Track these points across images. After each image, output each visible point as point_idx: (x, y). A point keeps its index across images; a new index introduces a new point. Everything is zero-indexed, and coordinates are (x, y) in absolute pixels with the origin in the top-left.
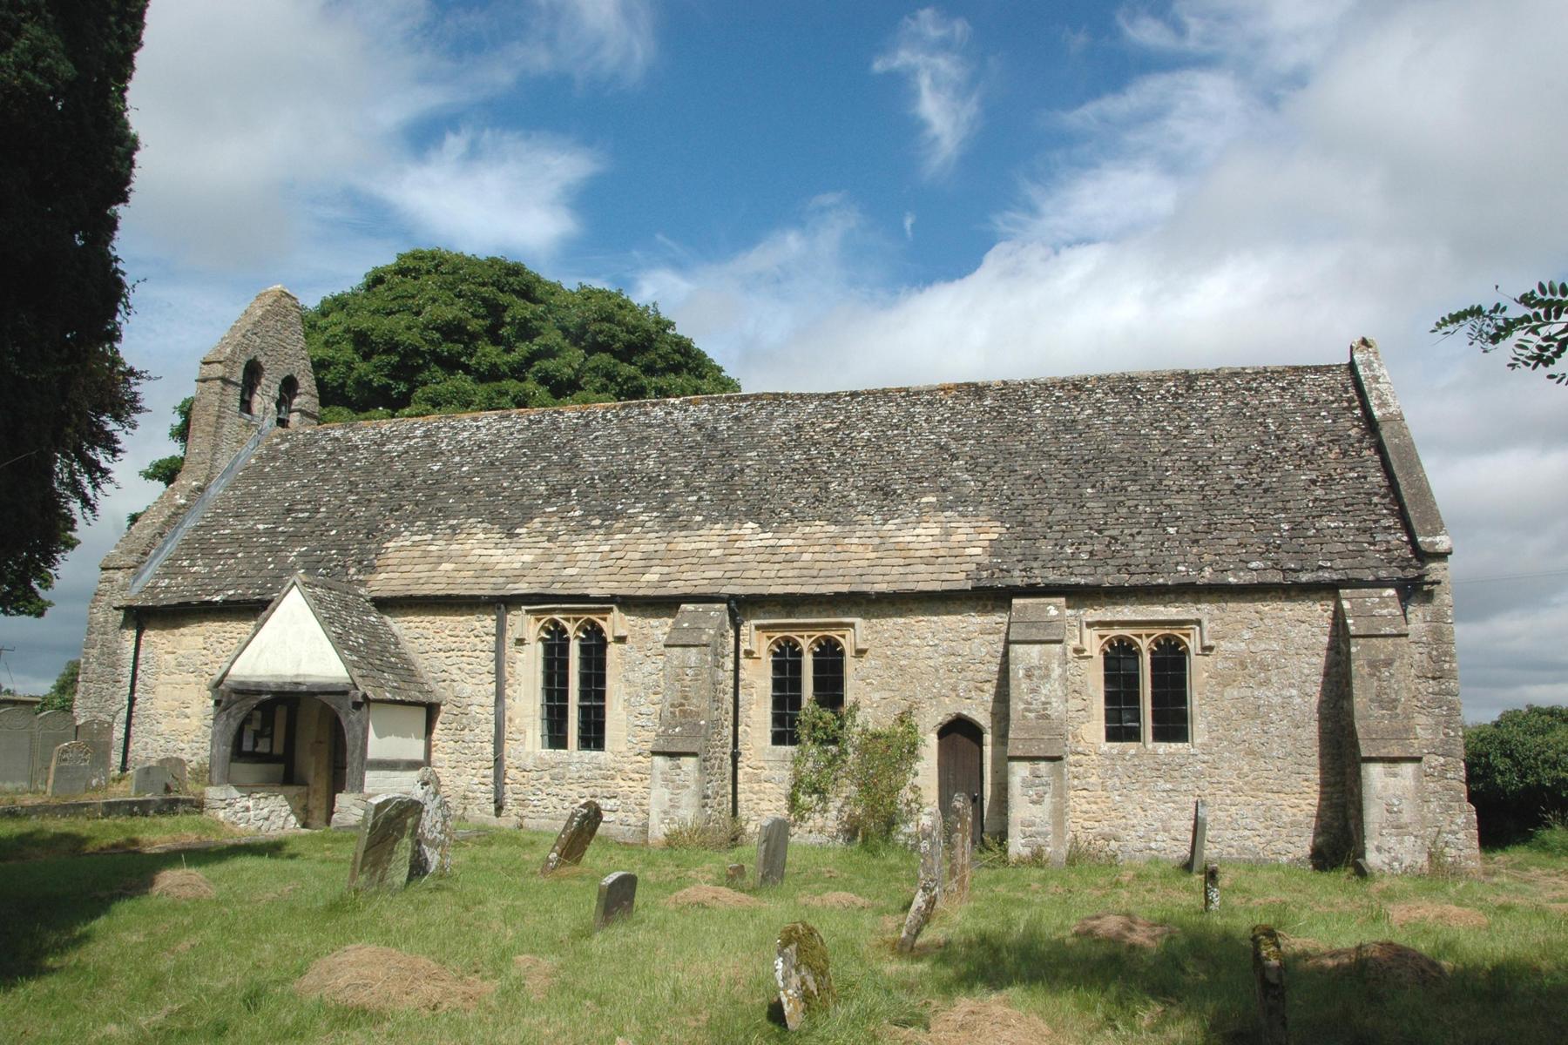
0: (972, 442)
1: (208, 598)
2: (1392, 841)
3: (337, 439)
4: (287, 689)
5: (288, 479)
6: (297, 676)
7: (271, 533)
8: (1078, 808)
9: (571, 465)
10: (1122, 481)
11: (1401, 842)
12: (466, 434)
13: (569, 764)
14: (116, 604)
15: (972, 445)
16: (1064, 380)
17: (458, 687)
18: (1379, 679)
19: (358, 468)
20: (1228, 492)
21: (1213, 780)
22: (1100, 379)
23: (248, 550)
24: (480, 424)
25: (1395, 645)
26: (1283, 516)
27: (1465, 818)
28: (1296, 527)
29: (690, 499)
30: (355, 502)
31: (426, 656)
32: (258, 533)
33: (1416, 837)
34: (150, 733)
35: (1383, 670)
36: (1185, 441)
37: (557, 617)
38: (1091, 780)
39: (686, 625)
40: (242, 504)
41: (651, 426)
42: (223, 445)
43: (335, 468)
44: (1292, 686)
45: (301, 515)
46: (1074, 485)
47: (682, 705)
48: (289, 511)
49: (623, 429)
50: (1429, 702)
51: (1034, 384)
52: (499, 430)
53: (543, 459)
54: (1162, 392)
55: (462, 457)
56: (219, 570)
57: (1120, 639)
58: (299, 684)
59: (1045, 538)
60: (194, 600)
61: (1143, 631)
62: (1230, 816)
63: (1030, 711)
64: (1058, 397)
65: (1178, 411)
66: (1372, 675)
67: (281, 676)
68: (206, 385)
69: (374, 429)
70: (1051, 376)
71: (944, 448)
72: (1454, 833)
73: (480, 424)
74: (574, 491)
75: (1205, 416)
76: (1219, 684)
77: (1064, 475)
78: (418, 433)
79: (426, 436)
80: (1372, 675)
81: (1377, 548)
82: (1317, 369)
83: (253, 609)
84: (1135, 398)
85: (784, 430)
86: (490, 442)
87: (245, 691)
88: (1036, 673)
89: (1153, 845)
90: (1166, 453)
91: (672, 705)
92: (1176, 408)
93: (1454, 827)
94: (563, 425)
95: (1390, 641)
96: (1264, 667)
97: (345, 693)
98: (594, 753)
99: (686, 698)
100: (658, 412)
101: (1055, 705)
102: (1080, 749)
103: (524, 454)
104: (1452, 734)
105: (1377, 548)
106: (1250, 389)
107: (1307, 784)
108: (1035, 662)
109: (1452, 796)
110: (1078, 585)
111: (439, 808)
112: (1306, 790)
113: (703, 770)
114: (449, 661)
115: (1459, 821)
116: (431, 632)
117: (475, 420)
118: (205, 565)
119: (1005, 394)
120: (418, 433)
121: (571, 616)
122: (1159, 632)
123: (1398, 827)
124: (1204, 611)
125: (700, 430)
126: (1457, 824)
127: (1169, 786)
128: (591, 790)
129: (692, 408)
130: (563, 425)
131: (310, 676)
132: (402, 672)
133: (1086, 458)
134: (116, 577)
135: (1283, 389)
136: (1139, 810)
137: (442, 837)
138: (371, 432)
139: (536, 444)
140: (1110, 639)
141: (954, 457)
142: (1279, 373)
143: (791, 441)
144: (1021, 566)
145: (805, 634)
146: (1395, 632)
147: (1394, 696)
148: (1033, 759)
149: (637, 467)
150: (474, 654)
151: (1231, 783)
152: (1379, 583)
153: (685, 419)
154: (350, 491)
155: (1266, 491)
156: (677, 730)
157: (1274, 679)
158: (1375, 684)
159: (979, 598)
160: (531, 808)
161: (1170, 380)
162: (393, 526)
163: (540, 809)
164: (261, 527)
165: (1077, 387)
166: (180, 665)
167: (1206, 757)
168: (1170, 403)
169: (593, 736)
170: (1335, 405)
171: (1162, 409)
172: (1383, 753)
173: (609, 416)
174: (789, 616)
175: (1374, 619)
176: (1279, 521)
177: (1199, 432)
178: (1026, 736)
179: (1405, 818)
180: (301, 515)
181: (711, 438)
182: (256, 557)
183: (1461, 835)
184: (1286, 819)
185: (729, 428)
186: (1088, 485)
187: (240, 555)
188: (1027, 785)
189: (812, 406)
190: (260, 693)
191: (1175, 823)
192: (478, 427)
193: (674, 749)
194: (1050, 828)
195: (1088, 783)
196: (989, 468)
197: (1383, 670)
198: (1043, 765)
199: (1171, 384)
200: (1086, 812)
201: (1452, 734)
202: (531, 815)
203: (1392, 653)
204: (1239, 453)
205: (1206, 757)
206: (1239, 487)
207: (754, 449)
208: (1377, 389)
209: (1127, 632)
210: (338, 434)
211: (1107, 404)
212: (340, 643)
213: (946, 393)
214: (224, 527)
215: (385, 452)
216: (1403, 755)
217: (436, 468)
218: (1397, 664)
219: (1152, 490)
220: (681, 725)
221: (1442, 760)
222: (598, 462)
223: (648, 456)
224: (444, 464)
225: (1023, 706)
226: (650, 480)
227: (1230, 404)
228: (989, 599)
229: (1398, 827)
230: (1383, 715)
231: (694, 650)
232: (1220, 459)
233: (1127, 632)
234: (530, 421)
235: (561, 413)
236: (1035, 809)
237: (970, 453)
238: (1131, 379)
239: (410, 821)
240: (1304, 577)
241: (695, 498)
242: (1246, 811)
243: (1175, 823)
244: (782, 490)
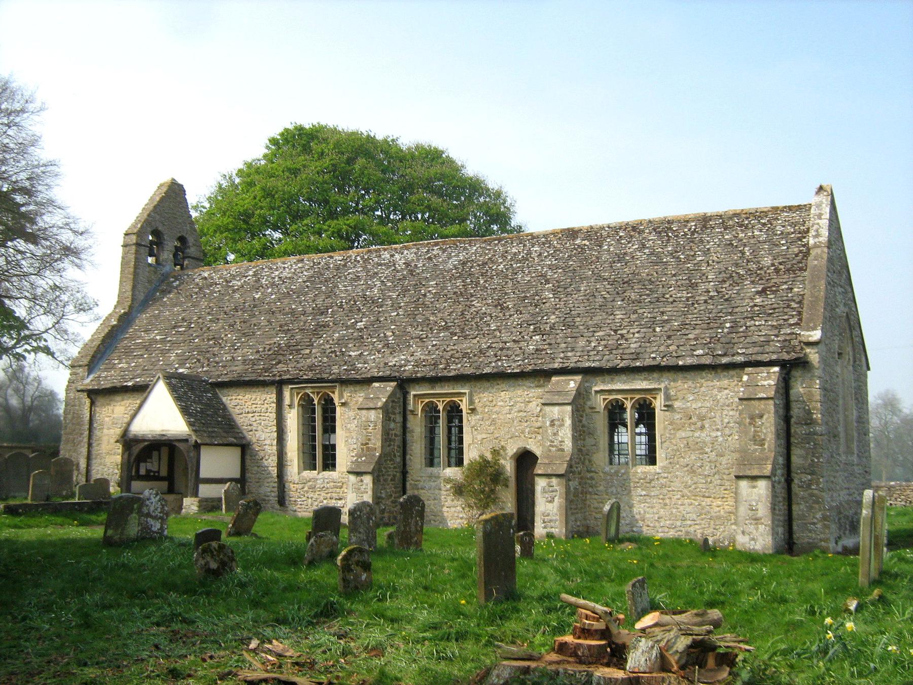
0: (560, 271)
1: (125, 384)
2: (751, 528)
3: (205, 278)
4: (158, 438)
5: (176, 305)
6: (163, 431)
7: (163, 341)
8: (592, 505)
9: (330, 294)
10: (640, 296)
11: (757, 529)
12: (277, 273)
13: (317, 480)
14: (80, 388)
15: (560, 273)
16: (627, 224)
17: (258, 434)
18: (755, 426)
19: (215, 298)
20: (702, 302)
21: (670, 489)
22: (650, 222)
23: (150, 353)
24: (286, 266)
25: (765, 405)
26: (729, 317)
27: (822, 514)
28: (735, 325)
29: (392, 314)
30: (211, 321)
31: (241, 416)
32: (156, 342)
33: (766, 525)
34: (100, 464)
35: (757, 420)
36: (689, 265)
37: (308, 391)
38: (599, 489)
39: (372, 396)
40: (149, 323)
41: (381, 265)
42: (139, 286)
43: (202, 298)
44: (718, 430)
45: (180, 330)
46: (611, 299)
47: (367, 444)
48: (175, 327)
49: (365, 268)
50: (802, 439)
51: (609, 227)
52: (295, 270)
53: (317, 289)
54: (686, 230)
55: (273, 289)
56: (134, 366)
57: (617, 400)
58: (163, 435)
59: (582, 336)
60: (118, 385)
61: (629, 396)
62: (680, 512)
63: (553, 446)
64: (621, 237)
65: (691, 244)
66: (750, 424)
67: (155, 431)
68: (128, 248)
69: (226, 270)
70: (620, 221)
71: (543, 276)
72: (814, 524)
73: (286, 266)
74: (330, 310)
75: (708, 247)
76: (674, 429)
77: (608, 292)
78: (251, 273)
79: (255, 275)
80: (750, 424)
81: (779, 339)
82: (790, 208)
83: (142, 390)
84: (667, 235)
85: (455, 266)
86: (290, 278)
87: (137, 440)
88: (556, 423)
89: (635, 529)
90: (674, 275)
91: (362, 444)
92: (691, 241)
93: (815, 521)
94: (332, 266)
95: (763, 402)
96: (702, 418)
97: (186, 441)
98: (331, 472)
99: (369, 440)
100: (386, 255)
101: (566, 442)
102: (593, 469)
103: (307, 286)
104: (816, 460)
105: (779, 339)
106: (741, 226)
107: (726, 492)
108: (556, 417)
109: (814, 500)
110: (589, 367)
111: (159, 501)
112: (726, 496)
113: (375, 482)
114: (254, 419)
115: (818, 516)
116: (243, 402)
117: (284, 263)
118: (127, 363)
119: (589, 236)
120: (251, 273)
121: (316, 390)
122: (638, 397)
123: (756, 519)
124: (661, 383)
125: (407, 267)
126: (816, 518)
127: (644, 493)
128: (329, 495)
129: (406, 252)
130: (332, 266)
131: (168, 430)
132: (225, 426)
133: (625, 280)
134: (79, 371)
135: (764, 225)
136: (627, 507)
137: (162, 515)
138: (225, 273)
139: (317, 277)
140: (610, 401)
141: (547, 282)
142: (764, 213)
143: (457, 273)
144: (562, 355)
145: (441, 400)
146: (765, 396)
147: (763, 437)
148: (549, 476)
149: (368, 293)
150: (267, 414)
151: (681, 491)
152: (771, 363)
153: (400, 260)
154: (209, 314)
155: (726, 300)
156: (363, 459)
157: (707, 426)
158: (753, 429)
159: (535, 376)
160: (299, 506)
161: (693, 221)
162: (229, 336)
163: (303, 506)
164: (158, 337)
165: (634, 228)
166: (113, 423)
167: (666, 475)
168: (688, 238)
169: (329, 463)
170: (793, 236)
171: (682, 243)
172: (749, 473)
173: (359, 258)
174: (433, 388)
175: (757, 387)
176: (725, 322)
177: (700, 258)
178: (547, 462)
179: (760, 513)
180: (180, 330)
181: (411, 272)
182: (153, 357)
183: (819, 526)
184: (713, 514)
185: (424, 265)
186: (620, 299)
187: (145, 356)
188: (544, 491)
189: (475, 248)
190: (145, 440)
191: (648, 516)
192: (284, 268)
193: (359, 470)
194: (558, 517)
195: (598, 491)
196: (565, 288)
197: (757, 420)
198: (554, 481)
199: (693, 224)
200: (596, 508)
201: (816, 460)
202: (299, 510)
203: (763, 410)
204: (720, 273)
205: (666, 475)
206: (711, 298)
207: (434, 280)
208: (818, 224)
209: (619, 397)
210: (206, 274)
211: (649, 240)
212: (185, 411)
213: (555, 236)
214: (139, 338)
215: (231, 286)
216: (759, 474)
217: (257, 296)
218: (765, 417)
219: (657, 301)
220: (366, 456)
221: (809, 477)
222: (347, 290)
223: (375, 285)
224: (262, 294)
225: (549, 444)
226: (373, 302)
227: (726, 237)
228: (541, 376)
229: (756, 519)
230: (757, 449)
231: (373, 411)
232: (707, 278)
233: (619, 397)
234: (314, 263)
235: (331, 257)
236: (550, 506)
237: (557, 279)
238: (669, 222)
239: (135, 506)
240: (724, 360)
241: (395, 313)
242: (689, 509)
243: (648, 516)
244: (445, 307)
